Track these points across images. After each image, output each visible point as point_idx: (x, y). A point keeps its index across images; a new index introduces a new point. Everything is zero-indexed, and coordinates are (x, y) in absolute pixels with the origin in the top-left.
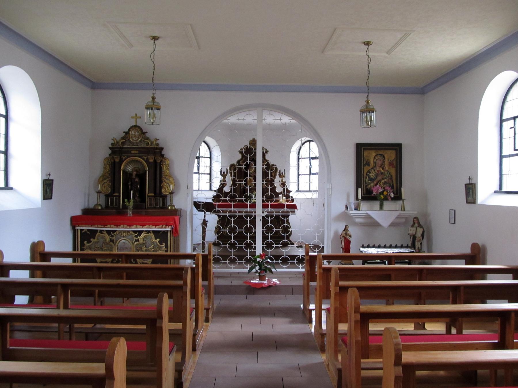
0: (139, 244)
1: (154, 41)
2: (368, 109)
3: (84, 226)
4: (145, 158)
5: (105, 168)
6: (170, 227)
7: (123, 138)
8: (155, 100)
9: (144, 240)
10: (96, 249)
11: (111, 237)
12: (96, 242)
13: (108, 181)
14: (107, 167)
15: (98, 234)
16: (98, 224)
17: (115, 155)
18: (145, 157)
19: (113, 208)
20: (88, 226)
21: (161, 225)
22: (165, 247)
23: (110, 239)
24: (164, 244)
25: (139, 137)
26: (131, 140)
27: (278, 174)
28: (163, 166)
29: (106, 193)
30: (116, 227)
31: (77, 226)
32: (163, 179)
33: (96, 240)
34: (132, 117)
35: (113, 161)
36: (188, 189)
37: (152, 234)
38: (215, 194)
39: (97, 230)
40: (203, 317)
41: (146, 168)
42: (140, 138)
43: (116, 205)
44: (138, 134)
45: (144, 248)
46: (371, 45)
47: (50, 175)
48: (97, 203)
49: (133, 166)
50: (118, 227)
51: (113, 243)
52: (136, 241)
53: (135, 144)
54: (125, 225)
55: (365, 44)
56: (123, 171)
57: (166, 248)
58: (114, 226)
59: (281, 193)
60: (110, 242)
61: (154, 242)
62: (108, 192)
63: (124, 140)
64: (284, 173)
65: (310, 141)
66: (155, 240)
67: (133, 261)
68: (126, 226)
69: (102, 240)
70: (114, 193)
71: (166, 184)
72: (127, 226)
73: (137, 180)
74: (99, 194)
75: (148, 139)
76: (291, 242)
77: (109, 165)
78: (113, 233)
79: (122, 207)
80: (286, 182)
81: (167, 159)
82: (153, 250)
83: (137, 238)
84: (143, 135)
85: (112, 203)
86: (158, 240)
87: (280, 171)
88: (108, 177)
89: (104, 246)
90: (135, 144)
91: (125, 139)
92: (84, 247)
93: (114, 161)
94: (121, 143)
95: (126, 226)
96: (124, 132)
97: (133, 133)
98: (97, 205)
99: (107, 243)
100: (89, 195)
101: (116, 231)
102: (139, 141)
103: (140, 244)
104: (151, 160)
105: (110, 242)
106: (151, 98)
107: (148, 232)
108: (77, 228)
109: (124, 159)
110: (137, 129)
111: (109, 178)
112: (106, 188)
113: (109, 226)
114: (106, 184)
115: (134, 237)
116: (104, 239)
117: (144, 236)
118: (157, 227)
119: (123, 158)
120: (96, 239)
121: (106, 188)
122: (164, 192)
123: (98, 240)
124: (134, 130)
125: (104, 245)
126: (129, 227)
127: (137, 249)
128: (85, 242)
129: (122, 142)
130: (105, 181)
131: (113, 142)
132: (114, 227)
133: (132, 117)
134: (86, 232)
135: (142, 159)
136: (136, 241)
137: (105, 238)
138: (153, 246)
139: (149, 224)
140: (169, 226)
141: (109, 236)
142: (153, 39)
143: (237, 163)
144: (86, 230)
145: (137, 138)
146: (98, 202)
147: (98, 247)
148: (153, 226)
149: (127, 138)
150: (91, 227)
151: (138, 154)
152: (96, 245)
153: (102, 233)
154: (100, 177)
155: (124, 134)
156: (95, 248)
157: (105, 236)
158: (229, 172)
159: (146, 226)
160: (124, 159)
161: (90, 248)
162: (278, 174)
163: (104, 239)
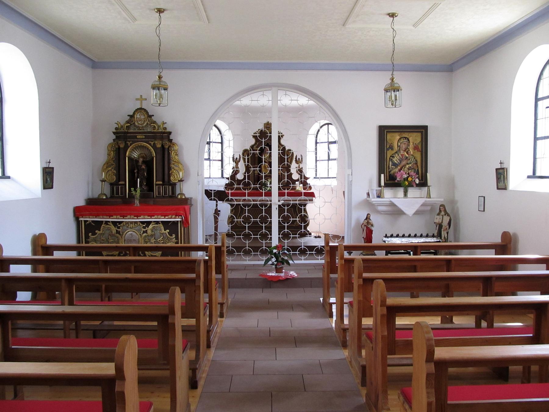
1: (160, 14)
2: (392, 88)
3: (88, 217)
4: (152, 143)
5: (109, 155)
7: (128, 122)
8: (162, 79)
9: (152, 232)
10: (101, 241)
12: (102, 234)
13: (112, 168)
14: (111, 153)
16: (103, 215)
17: (120, 141)
18: (152, 142)
24: (174, 236)
25: (145, 120)
26: (137, 125)
27: (294, 159)
30: (122, 218)
31: (81, 217)
33: (101, 232)
34: (137, 99)
35: (117, 147)
37: (161, 225)
38: (227, 182)
42: (146, 122)
46: (396, 16)
47: (49, 162)
48: (102, 192)
52: (144, 232)
55: (390, 16)
59: (298, 180)
63: (129, 124)
64: (300, 159)
65: (328, 124)
67: (141, 254)
68: (133, 216)
69: (108, 232)
73: (143, 167)
75: (155, 122)
77: (114, 151)
78: (119, 224)
79: (128, 196)
80: (284, 137)
82: (162, 241)
83: (145, 230)
85: (117, 193)
86: (168, 231)
87: (296, 156)
89: (110, 238)
90: (141, 128)
91: (130, 123)
92: (89, 240)
93: (119, 146)
95: (133, 216)
96: (129, 116)
97: (138, 116)
98: (102, 194)
102: (145, 125)
104: (159, 146)
106: (157, 77)
107: (157, 223)
109: (129, 145)
110: (142, 112)
113: (115, 217)
114: (110, 172)
118: (166, 217)
124: (139, 113)
126: (136, 218)
127: (146, 240)
130: (110, 169)
132: (120, 218)
133: (137, 99)
134: (90, 223)
135: (150, 145)
136: (144, 232)
138: (162, 237)
139: (158, 215)
141: (115, 228)
142: (158, 12)
144: (91, 222)
147: (104, 239)
148: (162, 216)
152: (101, 237)
154: (104, 164)
155: (129, 117)
157: (110, 228)
158: (241, 159)
160: (129, 145)
161: (95, 240)
162: (294, 159)
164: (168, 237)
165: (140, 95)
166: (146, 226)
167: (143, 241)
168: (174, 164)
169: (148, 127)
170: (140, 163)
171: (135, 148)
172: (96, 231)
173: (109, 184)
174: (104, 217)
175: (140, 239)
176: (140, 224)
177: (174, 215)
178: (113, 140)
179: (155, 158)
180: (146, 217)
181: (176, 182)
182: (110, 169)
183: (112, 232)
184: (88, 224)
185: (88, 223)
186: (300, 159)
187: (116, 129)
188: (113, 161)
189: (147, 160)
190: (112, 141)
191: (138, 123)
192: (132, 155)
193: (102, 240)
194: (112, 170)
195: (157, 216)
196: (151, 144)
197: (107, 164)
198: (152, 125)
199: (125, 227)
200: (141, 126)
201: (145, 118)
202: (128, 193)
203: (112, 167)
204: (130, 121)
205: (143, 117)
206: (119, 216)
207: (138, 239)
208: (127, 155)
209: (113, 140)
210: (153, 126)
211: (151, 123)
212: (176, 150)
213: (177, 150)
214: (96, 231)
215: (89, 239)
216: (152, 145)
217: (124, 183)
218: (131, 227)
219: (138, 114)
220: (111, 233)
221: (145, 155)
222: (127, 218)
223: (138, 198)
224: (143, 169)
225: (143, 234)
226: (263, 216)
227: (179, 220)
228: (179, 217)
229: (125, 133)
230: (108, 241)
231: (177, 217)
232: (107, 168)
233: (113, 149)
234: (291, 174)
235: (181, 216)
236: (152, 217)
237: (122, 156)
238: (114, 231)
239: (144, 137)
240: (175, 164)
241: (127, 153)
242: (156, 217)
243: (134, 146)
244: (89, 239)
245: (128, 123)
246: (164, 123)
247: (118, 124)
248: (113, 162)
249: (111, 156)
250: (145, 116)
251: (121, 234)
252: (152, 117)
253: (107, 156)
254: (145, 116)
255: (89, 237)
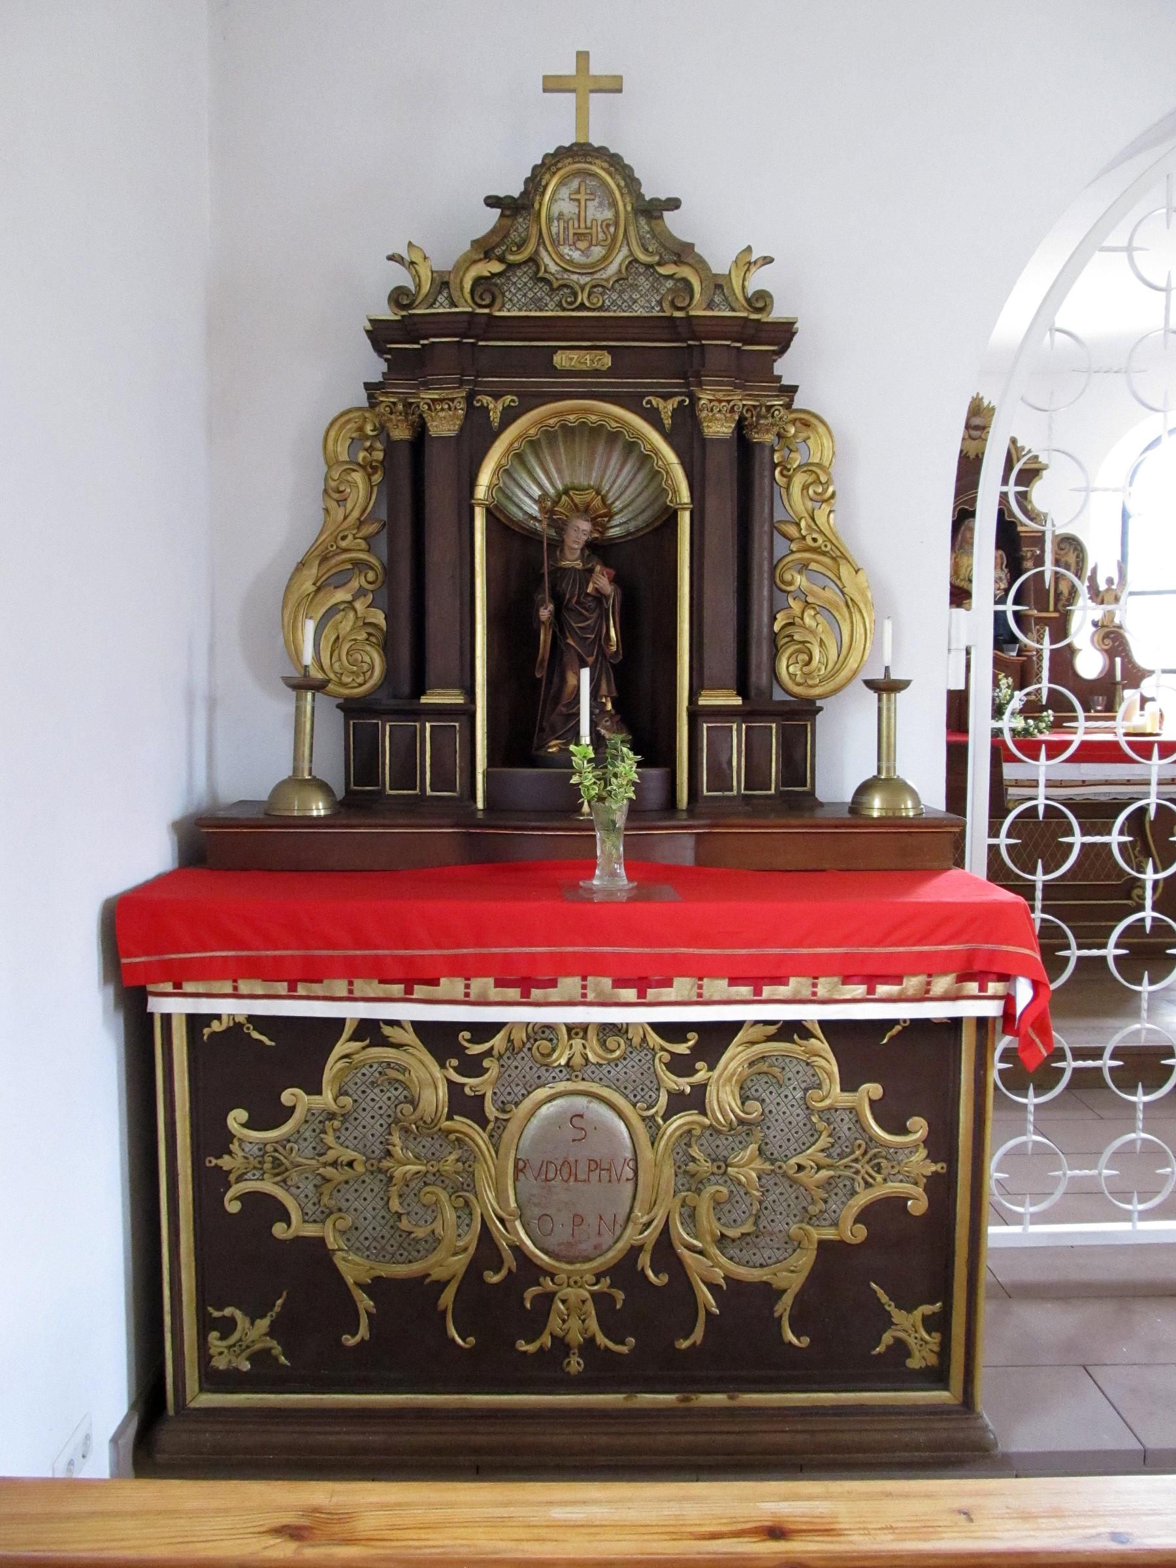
0: (705, 1127)
3: (227, 988)
4: (667, 408)
5: (334, 493)
6: (993, 987)
7: (485, 248)
9: (744, 1100)
10: (329, 1171)
11: (455, 1069)
12: (332, 1116)
13: (360, 593)
14: (353, 484)
15: (341, 1048)
16: (352, 970)
17: (426, 385)
18: (666, 397)
19: (416, 807)
20: (258, 987)
21: (914, 974)
22: (922, 1153)
23: (454, 1089)
24: (919, 1127)
25: (614, 238)
26: (553, 268)
28: (790, 479)
29: (346, 692)
30: (514, 993)
31: (168, 987)
32: (787, 577)
33: (327, 1098)
34: (552, 85)
35: (401, 433)
36: (953, 653)
37: (820, 1045)
39: (340, 1023)
40: (1008, 1527)
41: (676, 492)
42: (625, 251)
43: (442, 779)
44: (609, 214)
45: (751, 1161)
48: (295, 769)
49: (566, 473)
50: (536, 993)
51: (483, 1122)
52: (678, 1103)
53: (582, 297)
54: (603, 974)
56: (492, 515)
57: (935, 1162)
58: (499, 984)
60: (450, 1117)
61: (833, 1109)
62: (360, 680)
63: (496, 267)
64: (1116, 581)
66: (847, 1098)
67: (650, 1273)
68: (607, 982)
69: (382, 1099)
70: (420, 689)
71: (808, 620)
72: (619, 983)
73: (602, 582)
74: (309, 695)
75: (683, 253)
76: (623, 828)
77: (369, 468)
78: (474, 1041)
79: (487, 798)
81: (821, 429)
82: (824, 1173)
83: (684, 1084)
84: (643, 221)
85: (406, 774)
86: (873, 1090)
87: (1094, 571)
88: (360, 566)
89: (397, 1151)
90: (582, 297)
91: (501, 259)
92: (226, 1162)
93: (420, 430)
94: (468, 285)
95: (607, 982)
96: (492, 202)
97: (566, 207)
98: (295, 782)
99: (427, 1127)
100: (212, 704)
101: (493, 1028)
102: (613, 269)
103: (714, 1130)
104: (719, 428)
105: (450, 1117)
107: (791, 1030)
108: (158, 1006)
109: (495, 417)
110: (594, 175)
111: (371, 576)
112: (346, 647)
113: (451, 986)
114: (347, 623)
115: (660, 1069)
116: (401, 1093)
117: (751, 1064)
118: (882, 990)
119: (485, 410)
120: (328, 1094)
121: (346, 647)
122: (792, 676)
123: (346, 1101)
124: (575, 184)
125: (396, 1138)
126: (630, 994)
127: (692, 1167)
128: (236, 1118)
129: (478, 281)
130: (342, 596)
131: (402, 278)
132: (494, 993)
133: (552, 85)
134: (238, 1026)
135: (646, 419)
136: (678, 1103)
137: (406, 1088)
138: (824, 1141)
139: (815, 969)
140: (982, 977)
141: (443, 1066)
143: (1013, 522)
144: (242, 1020)
145: (598, 252)
146: (306, 765)
147: (352, 1154)
148: (847, 979)
149: (520, 246)
150: (292, 996)
151: (610, 372)
152: (329, 1139)
153: (385, 1042)
154: (302, 565)
155: (497, 212)
156: (325, 1165)
157: (404, 1070)
159: (786, 984)
160: (495, 417)
161: (276, 1163)
163: (401, 1093)
164: (872, 1139)
165: (579, 54)
166: (698, 1053)
167: (668, 1171)
168: (804, 567)
169: (634, 287)
170: (572, 559)
171: (534, 444)
172: (288, 1096)
173: (338, 706)
174: (362, 986)
175: (646, 1154)
176: (644, 1039)
177: (944, 973)
178: (368, 386)
179: (685, 520)
180: (718, 987)
181: (822, 697)
182: (342, 596)
183: (414, 1102)
184: (214, 1034)
185: (216, 1026)
186: (1116, 581)
187: (398, 297)
188: (365, 539)
189: (614, 532)
190: (361, 398)
191: (561, 256)
192: (509, 498)
193: (334, 1164)
194: (358, 605)
195: (806, 981)
196: (656, 410)
197: (324, 559)
198: (662, 270)
199: (523, 1064)
200: (583, 280)
201: (616, 224)
202: (488, 776)
203: (355, 584)
204: (502, 242)
205: (598, 213)
206: (490, 981)
207: (629, 1155)
208: (481, 492)
209: (368, 386)
210: (670, 284)
211: (657, 258)
212: (818, 465)
213: (827, 464)
214: (288, 1096)
215: (230, 1153)
216: (668, 422)
217: (462, 702)
218: (578, 1060)
219: (564, 192)
220: (408, 1108)
221: (597, 502)
222: (553, 994)
223: (620, 819)
224: (599, 597)
225: (666, 1118)
226: (1044, 867)
227: (992, 1009)
228: (982, 988)
229: (470, 325)
230: (380, 1170)
231: (972, 987)
232: (319, 589)
233: (361, 455)
234: (1071, 651)
235: (1004, 977)
236: (767, 991)
237: (439, 498)
238: (435, 1097)
239: (607, 361)
240: (813, 566)
241: (485, 478)
242: (796, 985)
243: (532, 431)
244: (230, 1153)
245: (488, 256)
246: (747, 262)
247: (412, 263)
248: (364, 545)
249: (349, 504)
250: (613, 205)
251: (491, 1111)
252: (667, 215)
253: (313, 506)
254: (613, 205)
255: (231, 1137)
